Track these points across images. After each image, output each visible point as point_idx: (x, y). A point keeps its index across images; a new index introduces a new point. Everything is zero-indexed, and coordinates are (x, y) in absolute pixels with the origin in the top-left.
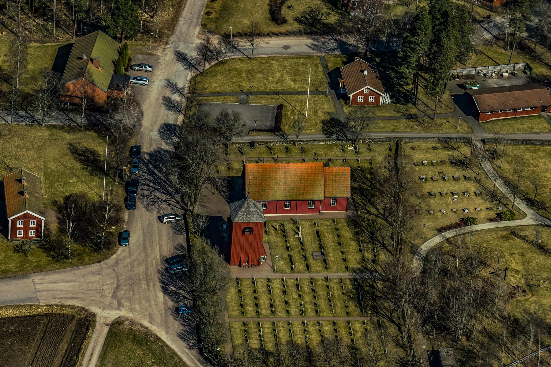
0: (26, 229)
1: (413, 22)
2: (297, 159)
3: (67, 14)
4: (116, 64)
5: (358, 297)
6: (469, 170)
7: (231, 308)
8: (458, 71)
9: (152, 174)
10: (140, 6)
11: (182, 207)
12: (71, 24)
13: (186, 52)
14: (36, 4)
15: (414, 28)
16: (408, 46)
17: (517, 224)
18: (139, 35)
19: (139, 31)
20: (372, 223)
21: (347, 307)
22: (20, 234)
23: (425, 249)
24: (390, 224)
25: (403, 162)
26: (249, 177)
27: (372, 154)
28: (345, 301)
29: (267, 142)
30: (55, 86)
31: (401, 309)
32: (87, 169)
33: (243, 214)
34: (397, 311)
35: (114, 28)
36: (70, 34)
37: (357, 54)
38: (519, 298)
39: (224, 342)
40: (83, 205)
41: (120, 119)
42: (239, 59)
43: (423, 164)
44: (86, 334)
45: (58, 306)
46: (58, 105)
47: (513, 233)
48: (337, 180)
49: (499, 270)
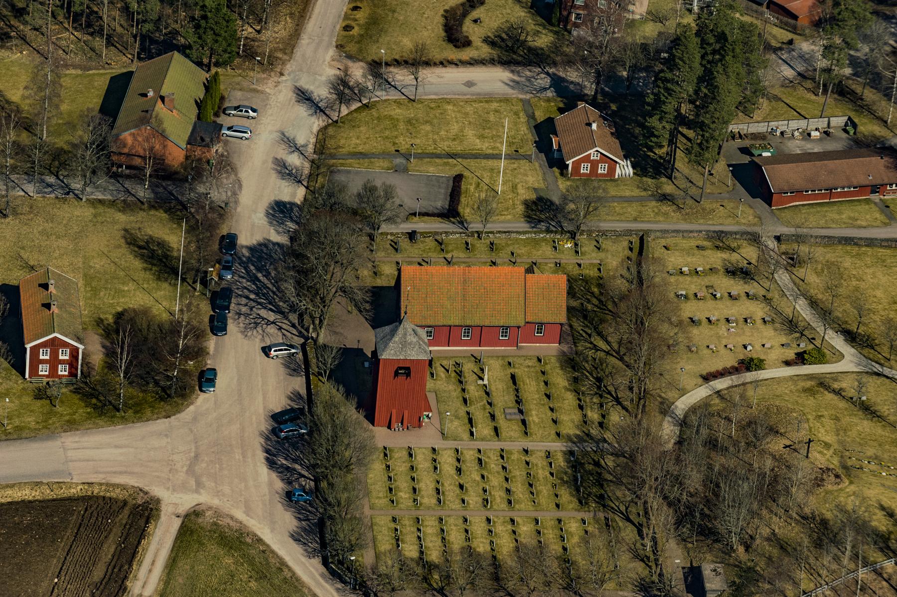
0: (54, 362)
1: (671, 48)
2: (483, 260)
3: (125, 25)
4: (199, 105)
5: (576, 480)
6: (755, 283)
7: (374, 494)
8: (741, 126)
9: (254, 279)
10: (240, 15)
11: (300, 332)
15: (672, 58)
16: (662, 85)
18: (237, 61)
19: (238, 53)
20: (598, 365)
21: (557, 496)
22: (44, 370)
23: (683, 407)
24: (627, 366)
25: (650, 269)
26: (406, 288)
27: (602, 255)
28: (554, 486)
29: (436, 233)
30: (104, 138)
31: (643, 501)
32: (151, 270)
33: (395, 345)
34: (636, 503)
36: (130, 56)
37: (582, 97)
39: (361, 547)
40: (145, 326)
41: (205, 192)
43: (681, 273)
44: (144, 530)
45: (101, 484)
46: (108, 168)
47: (821, 384)
48: (550, 300)
49: (799, 442)
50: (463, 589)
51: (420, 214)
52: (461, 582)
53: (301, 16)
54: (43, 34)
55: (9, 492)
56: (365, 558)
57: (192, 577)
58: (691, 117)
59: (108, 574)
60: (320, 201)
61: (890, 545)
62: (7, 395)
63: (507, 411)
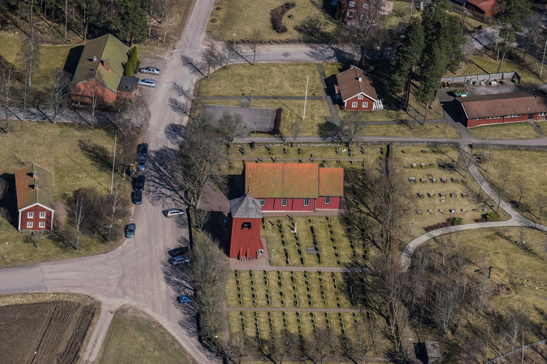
0: (36, 220)
1: (407, 32)
2: (294, 159)
3: (79, 17)
4: (125, 66)
5: (349, 290)
6: (457, 173)
7: (229, 298)
8: (448, 79)
9: (158, 171)
10: (149, 12)
11: (186, 202)
12: (82, 26)
13: (192, 57)
14: (48, 6)
15: (407, 38)
16: (401, 55)
17: (502, 225)
18: (147, 40)
19: (148, 36)
20: (362, 222)
21: (338, 299)
23: (413, 246)
24: (380, 222)
25: (393, 164)
26: (248, 176)
27: (364, 156)
28: (336, 293)
29: (266, 143)
30: (67, 86)
31: (389, 303)
32: (96, 165)
33: (242, 210)
34: (385, 304)
35: (123, 33)
36: (82, 36)
37: (353, 62)
38: (503, 295)
39: (222, 330)
40: (92, 198)
41: (128, 118)
42: (242, 65)
43: (412, 167)
44: (91, 321)
45: (65, 294)
46: (69, 104)
47: (497, 233)
48: (333, 184)
49: (484, 268)
50: (282, 355)
51: (257, 132)
52: (281, 351)
53: (185, 14)
54: (27, 22)
55: (7, 299)
56: (223, 337)
57: (119, 349)
58: (419, 74)
59: (68, 348)
60: (197, 124)
61: (542, 332)
62: (6, 240)
63: (308, 249)
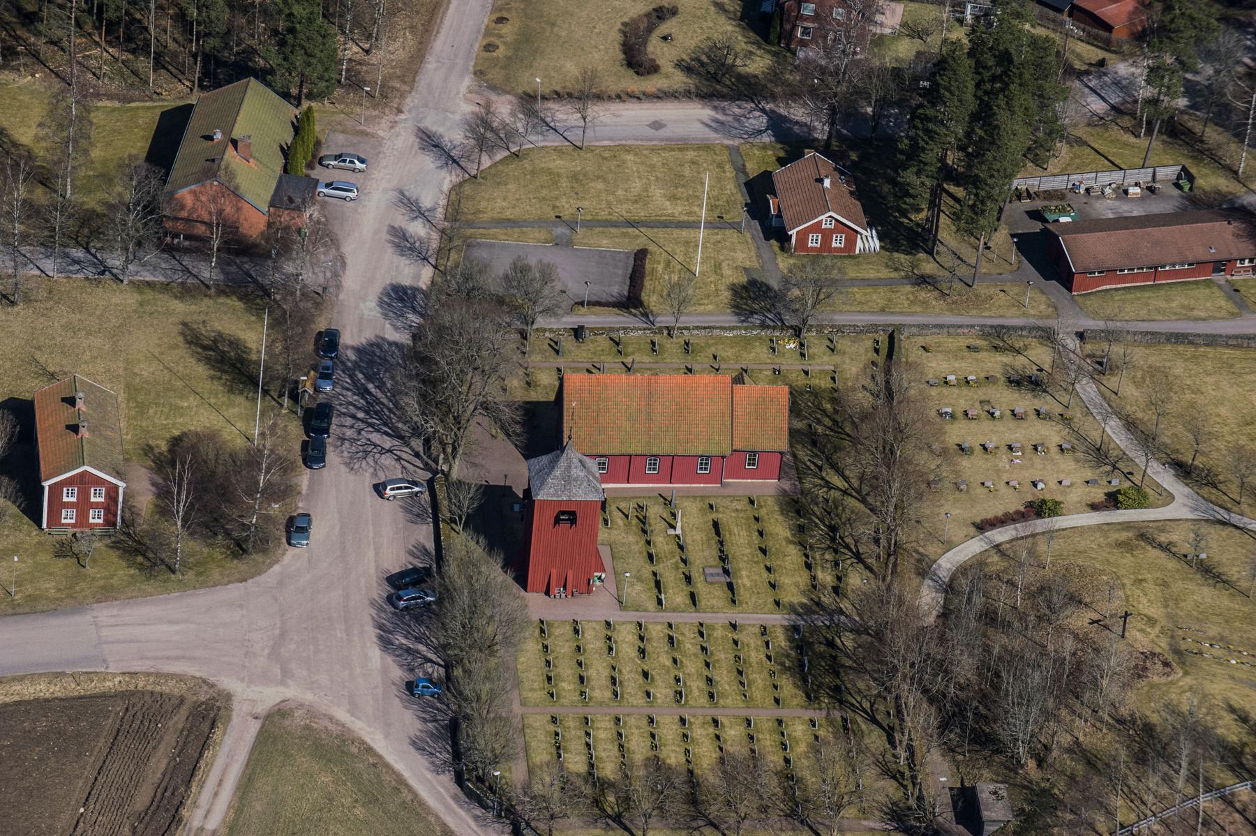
0: (83, 506)
1: (934, 74)
2: (676, 366)
3: (180, 39)
4: (286, 152)
5: (802, 666)
6: (1049, 397)
7: (527, 685)
8: (1030, 182)
9: (363, 392)
10: (342, 28)
11: (426, 464)
12: (189, 61)
13: (441, 130)
14: (110, 14)
15: (935, 87)
16: (920, 125)
17: (1152, 517)
18: (338, 92)
19: (339, 82)
20: (831, 509)
21: (776, 687)
23: (949, 566)
24: (872, 510)
25: (902, 377)
26: (570, 404)
27: (836, 359)
28: (772, 674)
29: (611, 329)
30: (154, 197)
31: (894, 695)
32: (220, 378)
33: (556, 481)
34: (885, 698)
35: (283, 75)
36: (188, 83)
37: (811, 143)
38: (1155, 678)
39: (509, 758)
40: (211, 455)
41: (295, 272)
42: (555, 149)
43: (946, 383)
44: (208, 738)
45: (148, 674)
46: (159, 238)
47: (1142, 536)
48: (765, 422)
49: (1111, 616)
50: (648, 816)
51: (589, 303)
52: (646, 806)
53: (426, 33)
54: (63, 50)
55: (17, 687)
56: (512, 774)
57: (274, 803)
58: (961, 169)
59: (156, 800)
60: (453, 284)
61: (1245, 762)
62: (15, 551)
63: (708, 571)
